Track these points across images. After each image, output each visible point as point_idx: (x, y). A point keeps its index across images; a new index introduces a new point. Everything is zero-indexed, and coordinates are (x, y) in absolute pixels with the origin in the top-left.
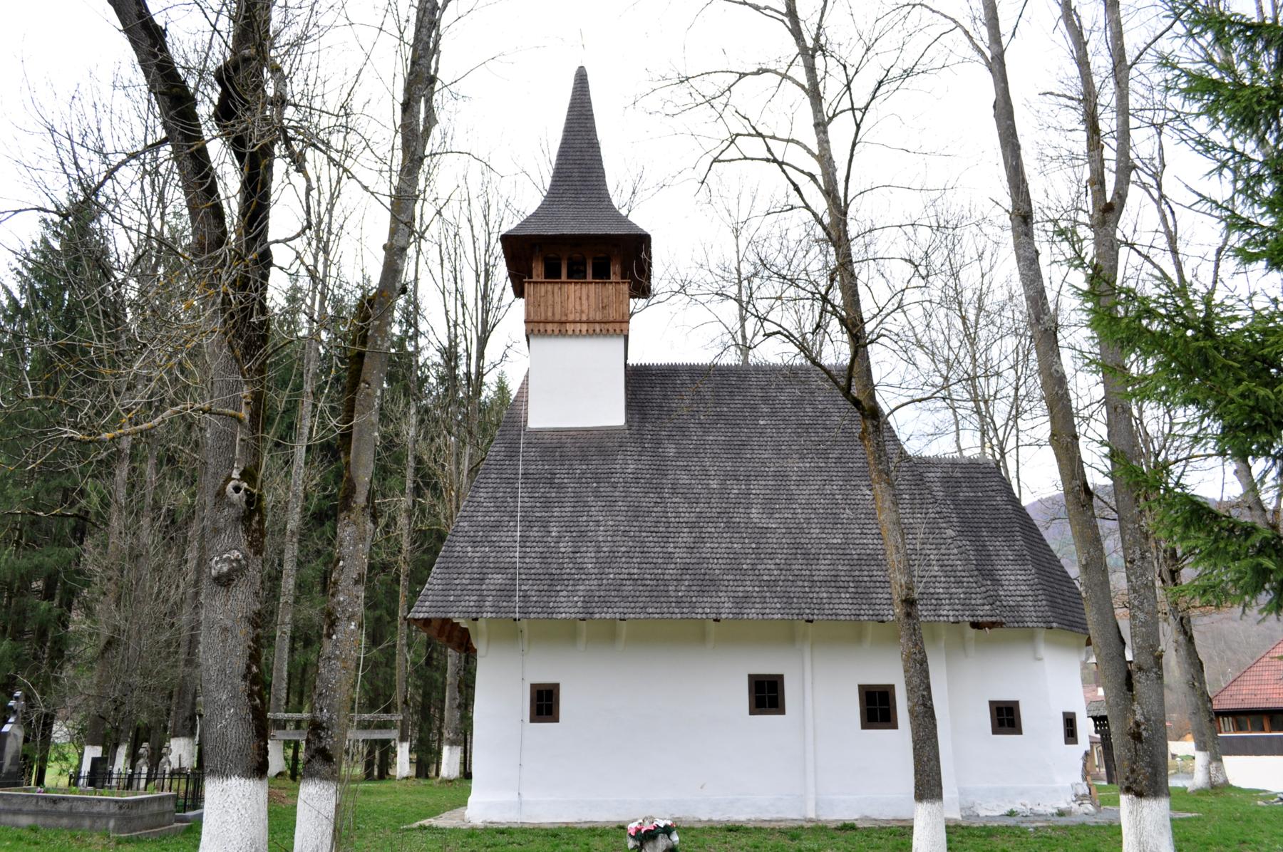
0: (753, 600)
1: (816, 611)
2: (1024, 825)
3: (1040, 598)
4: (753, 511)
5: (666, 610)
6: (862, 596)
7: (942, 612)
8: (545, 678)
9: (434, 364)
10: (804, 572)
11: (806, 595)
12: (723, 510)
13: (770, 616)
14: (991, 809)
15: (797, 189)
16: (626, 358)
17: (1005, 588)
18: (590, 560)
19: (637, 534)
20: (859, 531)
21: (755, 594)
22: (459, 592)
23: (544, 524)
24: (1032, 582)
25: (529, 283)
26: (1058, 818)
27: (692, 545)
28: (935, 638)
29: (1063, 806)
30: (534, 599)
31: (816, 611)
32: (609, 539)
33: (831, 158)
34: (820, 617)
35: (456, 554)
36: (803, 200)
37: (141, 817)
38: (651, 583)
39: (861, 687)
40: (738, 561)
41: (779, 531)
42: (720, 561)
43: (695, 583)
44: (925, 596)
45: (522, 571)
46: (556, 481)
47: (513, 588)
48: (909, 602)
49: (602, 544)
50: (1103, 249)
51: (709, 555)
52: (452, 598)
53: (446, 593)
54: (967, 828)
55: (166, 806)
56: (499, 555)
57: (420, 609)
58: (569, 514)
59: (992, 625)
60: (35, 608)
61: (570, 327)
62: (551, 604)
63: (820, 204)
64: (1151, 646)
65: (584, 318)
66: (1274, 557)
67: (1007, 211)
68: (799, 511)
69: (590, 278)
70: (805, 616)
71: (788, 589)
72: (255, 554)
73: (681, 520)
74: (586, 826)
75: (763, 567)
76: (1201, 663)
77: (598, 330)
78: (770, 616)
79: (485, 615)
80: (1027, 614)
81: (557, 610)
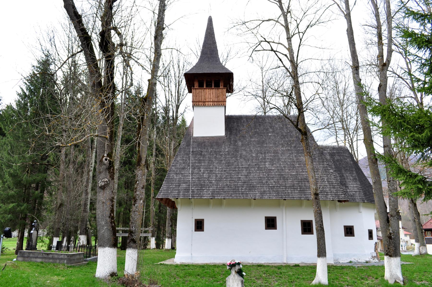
0: (266, 193)
1: (287, 196)
2: (354, 266)
3: (361, 192)
4: (267, 164)
5: (238, 196)
6: (302, 191)
7: (328, 197)
8: (199, 217)
9: (161, 113)
10: (283, 184)
11: (284, 191)
12: (257, 163)
13: (272, 198)
14: (344, 261)
15: (280, 60)
16: (225, 113)
17: (350, 189)
18: (214, 180)
19: (229, 171)
20: (301, 170)
21: (267, 191)
22: (172, 190)
23: (199, 168)
24: (358, 187)
25: (193, 89)
26: (366, 264)
27: (247, 175)
28: (326, 205)
29: (368, 260)
30: (196, 192)
31: (287, 196)
32: (220, 173)
33: (292, 49)
34: (288, 198)
35: (171, 178)
36: (283, 64)
37: (74, 260)
38: (234, 187)
39: (302, 221)
40: (262, 180)
41: (275, 170)
42: (256, 180)
43: (248, 187)
44: (323, 192)
45: (192, 183)
46: (203, 154)
47: (189, 188)
48: (316, 194)
49: (218, 174)
50: (382, 78)
51: (252, 178)
52: (169, 192)
53: (168, 190)
54: (335, 266)
55: (81, 256)
56: (184, 178)
57: (159, 195)
58: (207, 165)
59: (345, 201)
60: (34, 193)
61: (207, 103)
62: (201, 194)
63: (288, 64)
64: (395, 209)
65: (211, 100)
66: (423, 184)
67: (351, 66)
68: (282, 164)
69: (213, 87)
70: (283, 198)
71: (278, 189)
72: (112, 179)
73: (243, 167)
74: (213, 264)
75: (270, 182)
76: (419, 213)
77: (216, 104)
78: (272, 198)
79: (180, 197)
80: (357, 198)
81: (203, 196)
